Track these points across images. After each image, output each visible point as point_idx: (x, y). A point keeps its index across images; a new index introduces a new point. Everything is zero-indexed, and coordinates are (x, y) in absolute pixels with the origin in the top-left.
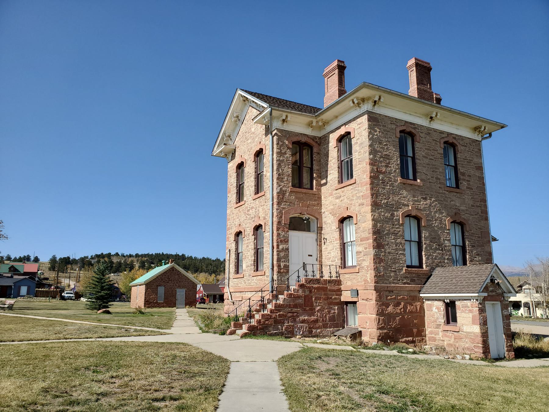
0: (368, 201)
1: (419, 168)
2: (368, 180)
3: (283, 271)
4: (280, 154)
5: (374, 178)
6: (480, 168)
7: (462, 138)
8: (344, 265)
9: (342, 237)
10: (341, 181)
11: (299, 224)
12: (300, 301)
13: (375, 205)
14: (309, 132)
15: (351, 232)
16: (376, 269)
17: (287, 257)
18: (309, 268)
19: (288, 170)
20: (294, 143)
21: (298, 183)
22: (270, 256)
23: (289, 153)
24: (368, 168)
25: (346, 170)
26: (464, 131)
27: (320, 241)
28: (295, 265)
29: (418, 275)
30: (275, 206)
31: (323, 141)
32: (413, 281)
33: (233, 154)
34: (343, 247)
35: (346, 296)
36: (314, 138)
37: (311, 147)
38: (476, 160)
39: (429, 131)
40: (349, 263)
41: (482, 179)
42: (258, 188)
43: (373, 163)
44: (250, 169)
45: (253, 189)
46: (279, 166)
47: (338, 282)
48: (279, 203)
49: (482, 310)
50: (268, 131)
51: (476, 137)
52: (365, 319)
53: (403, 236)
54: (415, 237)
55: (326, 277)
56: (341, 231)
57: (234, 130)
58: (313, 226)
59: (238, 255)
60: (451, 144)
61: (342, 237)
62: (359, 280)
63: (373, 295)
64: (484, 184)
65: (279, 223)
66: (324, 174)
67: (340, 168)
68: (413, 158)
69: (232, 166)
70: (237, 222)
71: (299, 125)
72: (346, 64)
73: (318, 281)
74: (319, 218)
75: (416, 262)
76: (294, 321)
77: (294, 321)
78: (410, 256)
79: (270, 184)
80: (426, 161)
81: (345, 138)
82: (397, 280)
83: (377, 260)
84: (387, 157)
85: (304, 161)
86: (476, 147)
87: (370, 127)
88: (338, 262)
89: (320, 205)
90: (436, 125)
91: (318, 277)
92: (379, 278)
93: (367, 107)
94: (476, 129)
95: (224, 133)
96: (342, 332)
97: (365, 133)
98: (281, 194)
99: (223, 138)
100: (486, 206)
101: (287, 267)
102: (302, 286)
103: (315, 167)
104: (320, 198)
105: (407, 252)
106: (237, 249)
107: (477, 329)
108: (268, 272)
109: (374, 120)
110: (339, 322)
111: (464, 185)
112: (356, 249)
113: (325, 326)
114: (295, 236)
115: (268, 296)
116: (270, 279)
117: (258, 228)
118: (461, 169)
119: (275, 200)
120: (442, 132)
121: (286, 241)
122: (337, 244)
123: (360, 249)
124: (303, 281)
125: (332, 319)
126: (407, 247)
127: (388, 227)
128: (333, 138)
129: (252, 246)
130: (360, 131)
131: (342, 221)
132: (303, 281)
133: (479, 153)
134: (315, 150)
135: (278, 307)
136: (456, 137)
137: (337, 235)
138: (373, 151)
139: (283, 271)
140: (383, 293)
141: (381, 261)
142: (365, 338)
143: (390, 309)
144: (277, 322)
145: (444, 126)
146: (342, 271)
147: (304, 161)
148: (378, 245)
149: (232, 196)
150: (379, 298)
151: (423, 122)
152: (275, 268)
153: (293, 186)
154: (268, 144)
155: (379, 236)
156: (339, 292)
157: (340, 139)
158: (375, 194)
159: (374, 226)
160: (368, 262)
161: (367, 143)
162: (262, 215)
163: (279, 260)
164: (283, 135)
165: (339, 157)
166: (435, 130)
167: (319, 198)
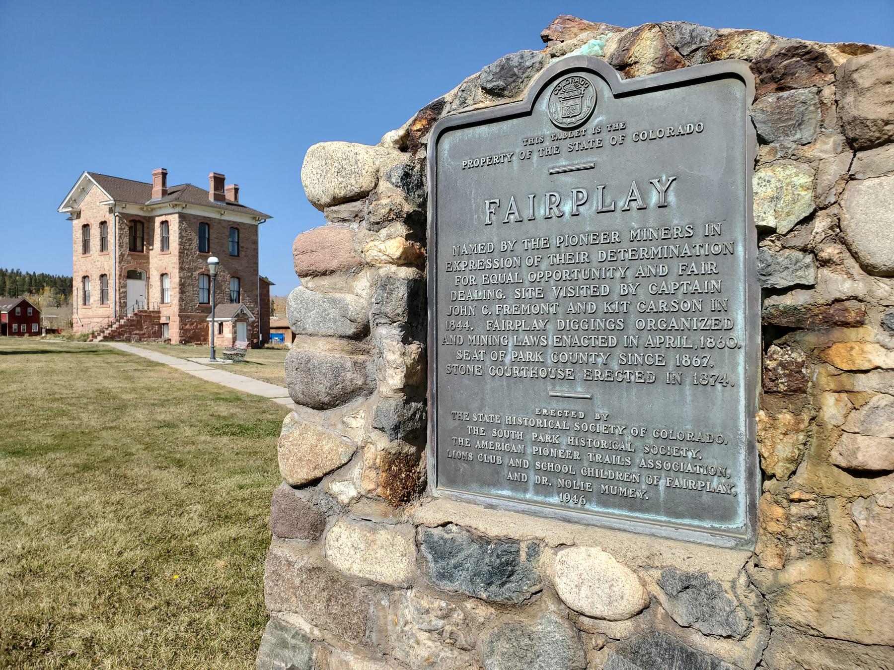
0: (177, 266)
1: (211, 245)
2: (177, 254)
3: (123, 306)
4: (121, 229)
5: (181, 253)
6: (256, 243)
7: (244, 224)
8: (163, 302)
9: (162, 285)
10: (162, 250)
11: (133, 275)
12: (135, 323)
13: (181, 269)
14: (141, 213)
15: (167, 283)
16: (180, 305)
17: (125, 297)
18: (140, 304)
19: (126, 240)
20: (130, 221)
21: (133, 248)
22: (113, 296)
23: (127, 229)
24: (178, 247)
25: (165, 242)
26: (246, 220)
27: (148, 286)
28: (131, 303)
29: (206, 308)
30: (117, 264)
31: (151, 220)
32: (203, 311)
33: (79, 215)
34: (163, 291)
35: (163, 320)
36: (144, 217)
37: (143, 223)
38: (253, 238)
39: (220, 221)
40: (166, 301)
41: (256, 250)
42: (103, 246)
43: (181, 244)
44: (95, 232)
45: (98, 248)
46: (120, 237)
47: (159, 312)
48: (120, 263)
49: (234, 327)
50: (111, 211)
51: (253, 222)
52: (173, 332)
53: (198, 286)
54: (206, 286)
55: (151, 309)
56: (162, 281)
57: (79, 196)
58: (144, 276)
59: (85, 292)
60: (235, 228)
61: (162, 285)
62: (170, 312)
63: (178, 319)
64: (257, 253)
65: (120, 275)
66: (151, 243)
67: (162, 241)
68: (208, 239)
69: (77, 224)
70: (84, 268)
71: (134, 210)
72: (168, 171)
73: (146, 311)
74: (147, 271)
75: (206, 301)
76: (130, 333)
77: (130, 333)
78: (203, 297)
79: (113, 248)
80: (217, 240)
81: (165, 223)
82: (192, 311)
83: (181, 299)
84: (190, 240)
85: (138, 233)
86: (254, 229)
87: (180, 222)
88: (159, 300)
89: (148, 262)
90: (224, 218)
91: (146, 308)
92: (181, 310)
93: (178, 209)
94: (254, 218)
95: (71, 198)
96: (160, 340)
97: (177, 225)
98: (122, 255)
99: (69, 201)
100: (257, 267)
101: (125, 303)
102: (135, 314)
103: (145, 237)
104: (148, 258)
105: (201, 295)
106: (84, 288)
107: (230, 336)
108: (112, 305)
109: (183, 217)
110: (159, 334)
111: (242, 254)
112: (170, 293)
113: (149, 337)
114: (130, 282)
115: (112, 319)
116: (114, 310)
117: (103, 276)
118: (241, 244)
119: (118, 260)
120: (229, 221)
121: (125, 286)
122: (159, 289)
123: (172, 293)
124: (136, 311)
125: (154, 333)
126: (201, 292)
127: (189, 281)
128: (158, 221)
129: (98, 287)
130: (174, 221)
131: (162, 275)
132: (136, 311)
133: (257, 231)
134: (145, 225)
135: (121, 326)
136: (239, 224)
137: (159, 284)
138: (181, 237)
139: (123, 306)
140: (183, 318)
141: (183, 300)
142: (173, 342)
143: (188, 327)
144: (120, 334)
145: (231, 217)
146: (161, 305)
147: (138, 233)
148: (182, 292)
149: (79, 247)
150: (181, 321)
151: (217, 216)
152: (118, 304)
153: (130, 250)
154: (112, 220)
155: (183, 287)
156: (159, 317)
157: (162, 223)
158: (181, 262)
159: (180, 281)
160: (176, 301)
161: (178, 231)
162: (107, 267)
163: (120, 298)
164: (123, 216)
165: (162, 233)
166: (225, 221)
167: (147, 258)
